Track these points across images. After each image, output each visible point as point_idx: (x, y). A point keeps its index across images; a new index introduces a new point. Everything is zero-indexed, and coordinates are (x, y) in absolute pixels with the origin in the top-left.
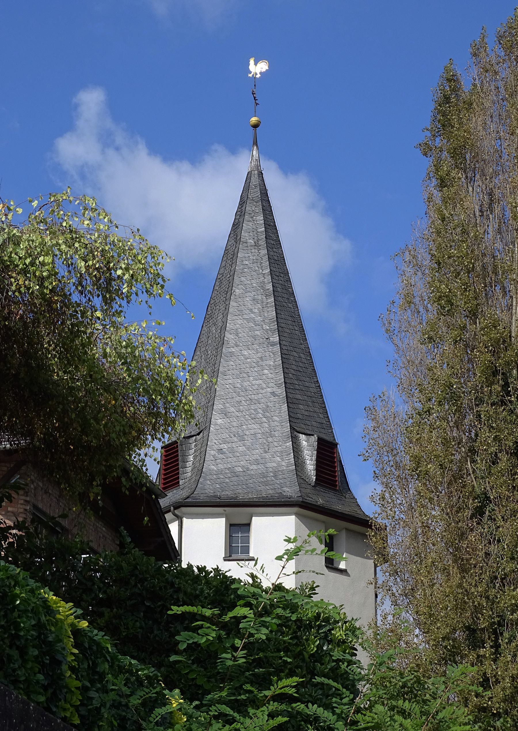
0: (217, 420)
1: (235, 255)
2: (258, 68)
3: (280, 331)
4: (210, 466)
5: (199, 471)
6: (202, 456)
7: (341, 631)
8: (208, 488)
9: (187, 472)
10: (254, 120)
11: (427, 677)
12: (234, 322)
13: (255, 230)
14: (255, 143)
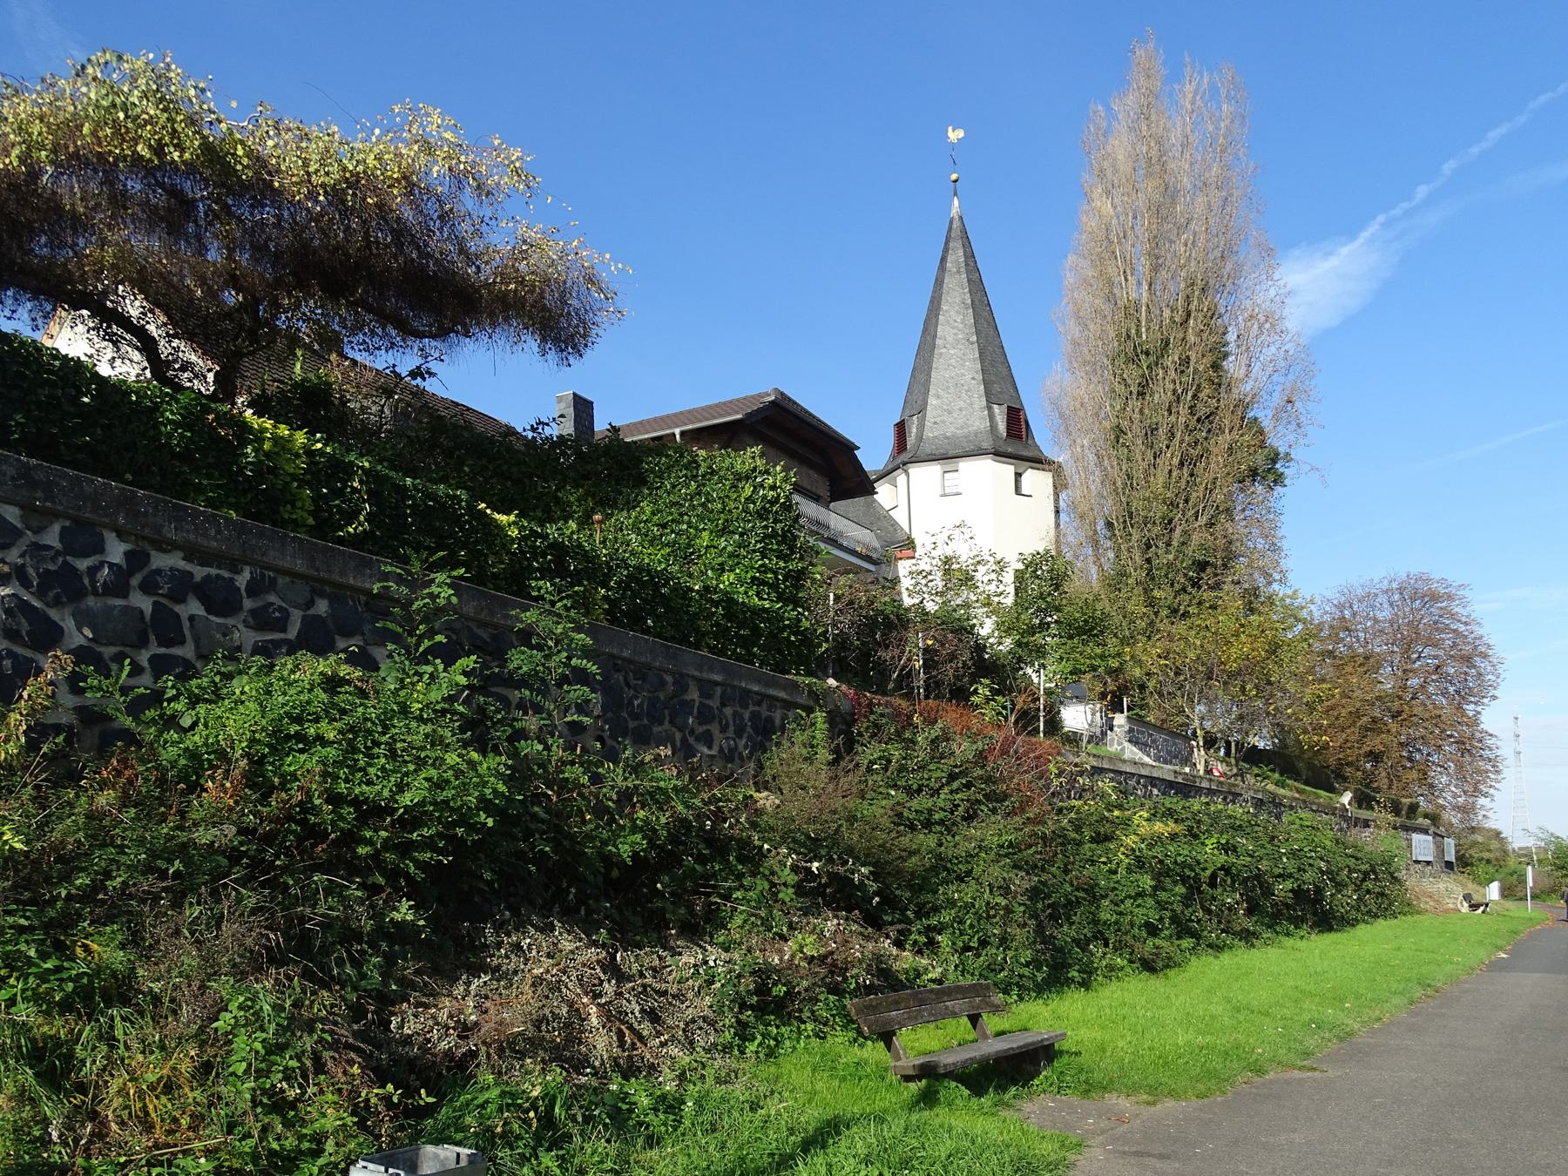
0: (932, 401)
1: (942, 282)
2: (955, 135)
3: (978, 333)
4: (928, 434)
5: (920, 438)
6: (921, 426)
7: (1183, 410)
8: (927, 448)
9: (911, 440)
10: (954, 177)
11: (155, 1007)
12: (941, 330)
13: (957, 261)
14: (955, 194)
